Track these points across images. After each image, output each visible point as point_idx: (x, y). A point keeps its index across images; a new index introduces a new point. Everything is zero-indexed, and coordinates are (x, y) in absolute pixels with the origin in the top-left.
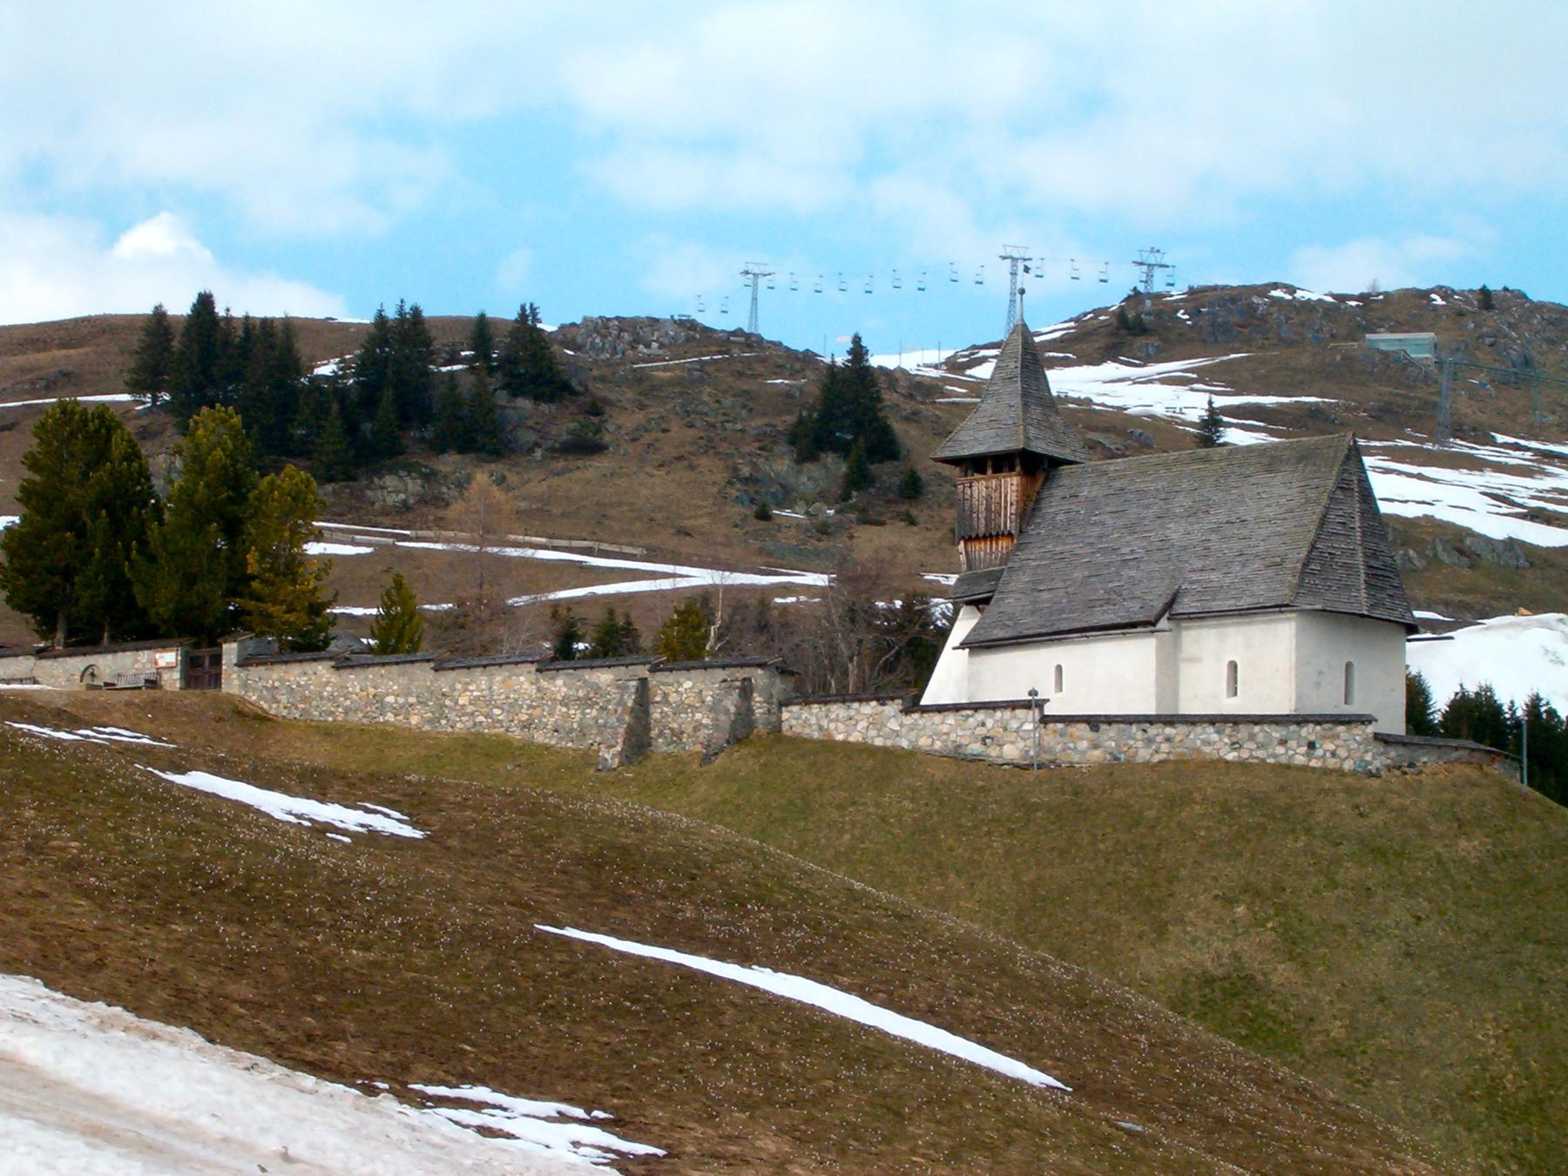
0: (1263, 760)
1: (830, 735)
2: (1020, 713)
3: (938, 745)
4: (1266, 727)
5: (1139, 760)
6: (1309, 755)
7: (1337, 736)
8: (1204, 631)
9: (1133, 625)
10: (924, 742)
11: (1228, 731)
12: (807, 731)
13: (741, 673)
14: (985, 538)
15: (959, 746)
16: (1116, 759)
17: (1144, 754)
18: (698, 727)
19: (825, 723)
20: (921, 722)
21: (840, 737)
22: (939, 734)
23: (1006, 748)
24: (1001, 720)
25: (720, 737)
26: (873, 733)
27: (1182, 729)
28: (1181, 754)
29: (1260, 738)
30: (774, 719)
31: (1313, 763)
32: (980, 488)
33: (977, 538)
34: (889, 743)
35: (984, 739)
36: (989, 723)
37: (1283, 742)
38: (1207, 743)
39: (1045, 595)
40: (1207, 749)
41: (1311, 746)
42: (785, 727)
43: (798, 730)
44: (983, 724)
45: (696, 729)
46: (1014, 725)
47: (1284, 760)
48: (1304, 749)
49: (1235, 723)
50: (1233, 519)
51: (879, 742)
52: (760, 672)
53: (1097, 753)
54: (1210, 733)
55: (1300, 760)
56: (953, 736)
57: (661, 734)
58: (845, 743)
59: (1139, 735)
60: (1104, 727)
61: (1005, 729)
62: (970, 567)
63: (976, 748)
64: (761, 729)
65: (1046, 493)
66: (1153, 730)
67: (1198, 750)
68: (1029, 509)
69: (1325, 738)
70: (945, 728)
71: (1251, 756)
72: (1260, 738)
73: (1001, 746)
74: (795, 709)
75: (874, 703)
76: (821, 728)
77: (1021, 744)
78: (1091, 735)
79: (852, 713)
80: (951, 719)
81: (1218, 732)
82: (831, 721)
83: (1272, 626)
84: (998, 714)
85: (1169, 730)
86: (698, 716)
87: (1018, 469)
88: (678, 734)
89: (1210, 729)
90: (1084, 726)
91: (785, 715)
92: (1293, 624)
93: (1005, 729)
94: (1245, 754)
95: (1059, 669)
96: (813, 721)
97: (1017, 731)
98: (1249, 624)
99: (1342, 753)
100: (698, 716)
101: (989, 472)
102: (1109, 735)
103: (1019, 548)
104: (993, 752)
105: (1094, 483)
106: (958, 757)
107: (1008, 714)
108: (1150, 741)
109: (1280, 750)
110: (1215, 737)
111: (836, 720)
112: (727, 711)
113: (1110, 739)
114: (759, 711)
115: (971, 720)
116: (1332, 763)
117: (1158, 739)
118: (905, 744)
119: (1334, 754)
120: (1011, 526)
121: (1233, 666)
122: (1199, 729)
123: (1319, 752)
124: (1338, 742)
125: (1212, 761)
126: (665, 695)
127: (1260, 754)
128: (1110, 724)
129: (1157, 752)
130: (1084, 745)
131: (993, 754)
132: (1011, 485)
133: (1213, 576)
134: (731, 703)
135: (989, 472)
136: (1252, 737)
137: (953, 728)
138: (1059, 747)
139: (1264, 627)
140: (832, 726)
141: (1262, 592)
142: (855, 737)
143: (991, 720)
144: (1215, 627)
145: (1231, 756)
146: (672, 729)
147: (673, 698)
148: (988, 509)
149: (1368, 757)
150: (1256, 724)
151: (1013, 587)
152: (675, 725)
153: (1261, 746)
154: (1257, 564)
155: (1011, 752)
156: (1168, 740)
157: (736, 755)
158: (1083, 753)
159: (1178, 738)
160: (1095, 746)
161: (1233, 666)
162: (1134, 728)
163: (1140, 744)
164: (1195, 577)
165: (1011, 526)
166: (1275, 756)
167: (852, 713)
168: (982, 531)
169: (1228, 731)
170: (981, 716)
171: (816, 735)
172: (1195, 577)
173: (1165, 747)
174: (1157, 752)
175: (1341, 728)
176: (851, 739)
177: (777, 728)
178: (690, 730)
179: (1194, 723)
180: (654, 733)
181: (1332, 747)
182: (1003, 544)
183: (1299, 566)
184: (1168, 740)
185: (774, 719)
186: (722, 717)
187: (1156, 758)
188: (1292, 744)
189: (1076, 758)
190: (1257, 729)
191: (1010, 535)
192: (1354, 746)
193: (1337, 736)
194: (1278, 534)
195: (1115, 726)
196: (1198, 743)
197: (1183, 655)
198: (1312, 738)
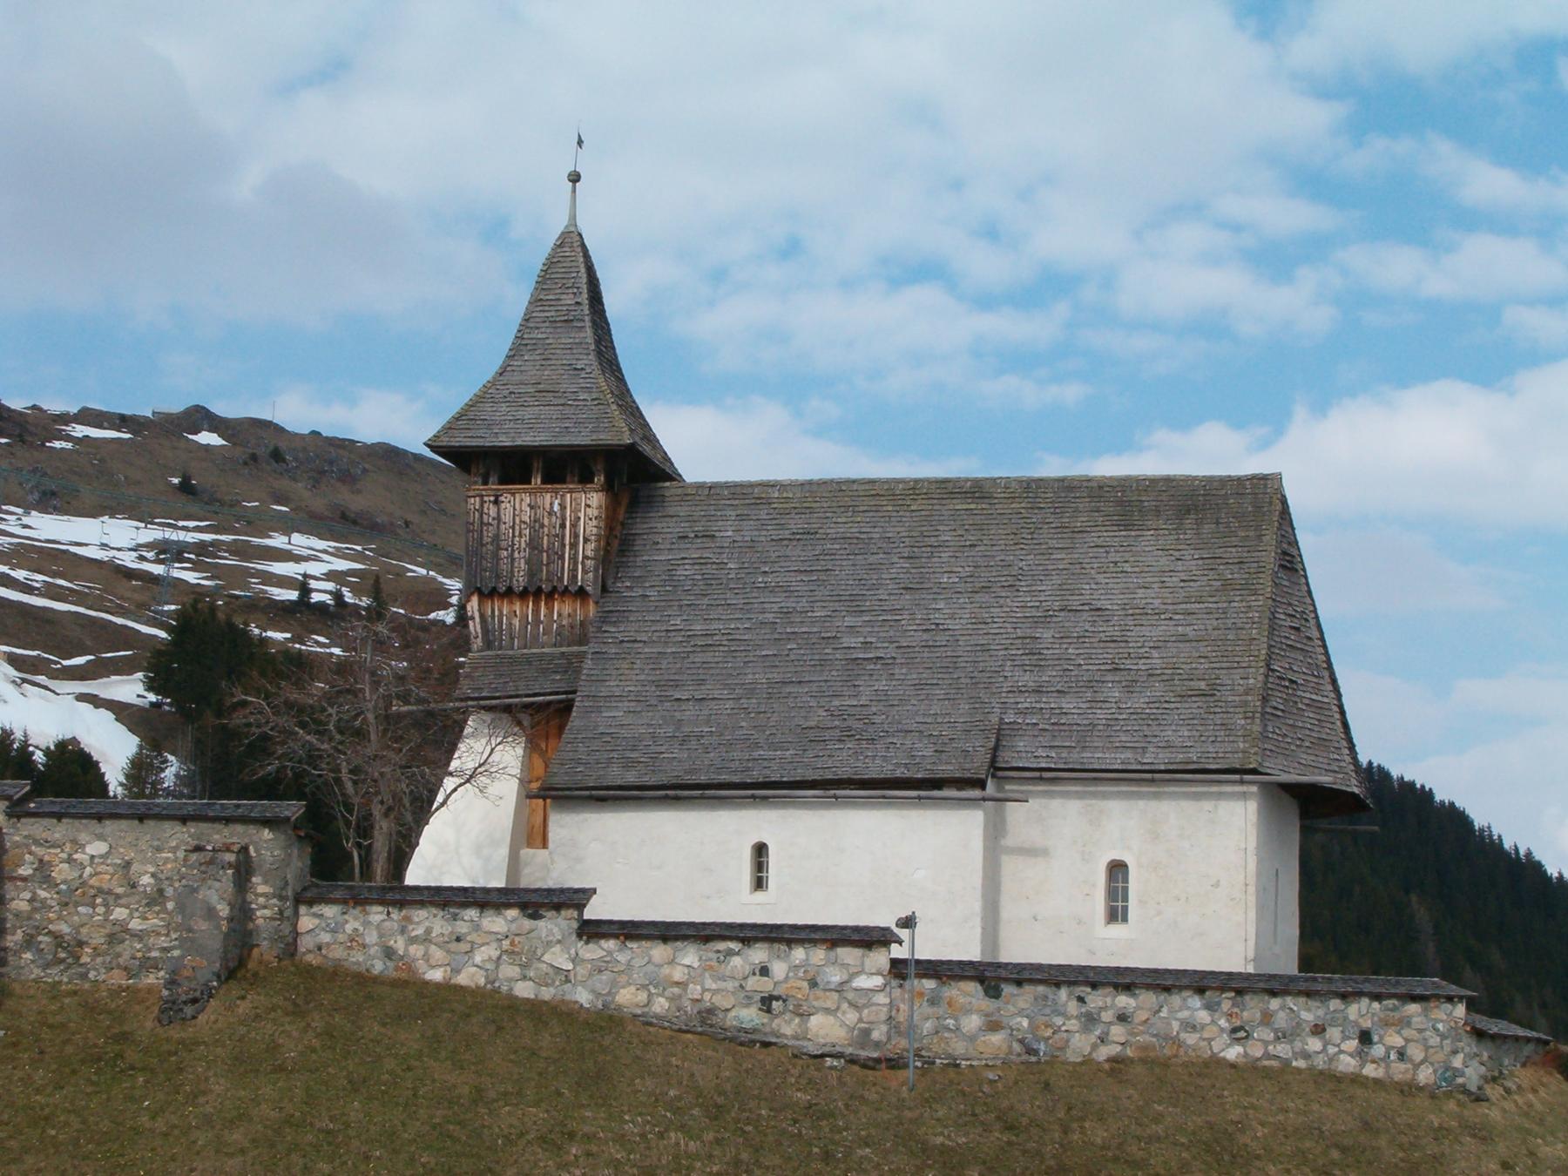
0: (1286, 1063)
1: (410, 968)
2: (848, 954)
3: (660, 1005)
4: (1289, 1001)
5: (1073, 1058)
6: (1360, 1055)
7: (1405, 1022)
8: (1056, 804)
9: (937, 784)
10: (628, 997)
11: (1226, 1006)
12: (357, 957)
13: (236, 834)
14: (524, 595)
15: (711, 1011)
16: (1031, 1051)
17: (1080, 1044)
18: (117, 935)
19: (399, 944)
20: (622, 958)
21: (436, 975)
22: (664, 984)
23: (815, 1021)
24: (805, 964)
25: (204, 966)
26: (509, 971)
27: (1148, 998)
28: (1145, 1048)
29: (1281, 1020)
30: (286, 929)
31: (1370, 1071)
32: (517, 509)
33: (509, 593)
34: (547, 994)
35: (767, 1002)
36: (779, 969)
37: (1319, 1030)
38: (1191, 1026)
39: (690, 711)
40: (1191, 1039)
41: (1365, 1038)
42: (305, 943)
43: (338, 953)
44: (765, 971)
45: (112, 939)
46: (835, 976)
47: (1320, 1063)
48: (1352, 1044)
49: (1240, 992)
50: (1075, 605)
51: (524, 990)
52: (267, 834)
53: (997, 1038)
54: (1194, 1007)
55: (1347, 1064)
56: (694, 990)
57: (29, 942)
58: (448, 990)
59: (1073, 1007)
60: (1008, 989)
61: (813, 984)
62: (488, 644)
63: (749, 1016)
64: (265, 950)
65: (640, 528)
66: (1096, 1000)
67: (1177, 1042)
68: (617, 546)
69: (1386, 1024)
70: (678, 974)
71: (1267, 1056)
72: (1281, 1020)
73: (804, 1016)
74: (330, 911)
75: (512, 913)
76: (389, 953)
77: (851, 1017)
78: (988, 1004)
79: (462, 928)
80: (690, 956)
81: (1209, 1007)
82: (413, 940)
83: (1207, 805)
84: (799, 954)
85: (1123, 1001)
86: (120, 913)
87: (599, 479)
88: (69, 948)
89: (1196, 1001)
90: (973, 987)
91: (306, 922)
92: (1252, 806)
93: (813, 984)
94: (1257, 1051)
95: (760, 850)
96: (371, 938)
97: (840, 989)
98: (1157, 796)
99: (1416, 1053)
100: (120, 913)
101: (537, 480)
102: (1019, 1005)
103: (605, 618)
104: (787, 1027)
105: (741, 517)
106: (705, 1026)
107: (819, 954)
108: (1090, 1020)
109: (1314, 1044)
110: (1203, 1016)
111: (426, 939)
112: (211, 913)
113: (1021, 1013)
114: (264, 913)
115: (736, 961)
116: (1399, 1071)
117: (1107, 1016)
118: (583, 997)
119: (1402, 1055)
120: (586, 577)
121: (1117, 870)
122: (1176, 1000)
123: (1378, 1050)
124: (1406, 1032)
125: (1206, 1064)
126: (43, 866)
127: (1282, 1050)
128: (1019, 983)
129: (1103, 1040)
130: (972, 1022)
131: (788, 1030)
132: (585, 507)
133: (1068, 703)
134: (217, 895)
135: (537, 480)
136: (1267, 1018)
137: (693, 975)
138: (928, 1026)
139: (1188, 806)
140: (416, 951)
141: (1179, 738)
142: (468, 977)
143: (785, 966)
144: (1080, 796)
145: (1233, 1053)
146: (57, 937)
147: (62, 872)
148: (534, 545)
149: (1457, 1062)
150: (1273, 993)
151: (613, 686)
152: (65, 928)
153: (1282, 1036)
154: (1158, 689)
155: (826, 1029)
156: (1122, 1018)
157: (243, 1008)
158: (972, 1038)
159: (1142, 1016)
160: (993, 1026)
161: (1117, 870)
162: (1063, 993)
163: (1073, 1024)
164: (1026, 702)
165: (586, 577)
166: (1306, 1056)
167: (462, 928)
168: (520, 581)
169: (1226, 1006)
170: (759, 954)
171: (378, 967)
172: (1026, 702)
173: (1118, 1032)
174: (1103, 1040)
175: (1413, 1008)
176: (462, 979)
177: (290, 948)
178: (98, 939)
179: (1167, 989)
180: (14, 939)
181: (1397, 1041)
182: (563, 610)
183: (1254, 701)
184: (1122, 1018)
185: (286, 929)
186: (202, 925)
187: (1104, 1053)
188: (1334, 1033)
189: (959, 1047)
190: (1275, 1003)
191: (582, 593)
192: (1434, 1040)
193: (1405, 1022)
194: (1184, 639)
195: (1028, 988)
196: (1176, 1025)
197: (1009, 841)
198: (1366, 1024)
